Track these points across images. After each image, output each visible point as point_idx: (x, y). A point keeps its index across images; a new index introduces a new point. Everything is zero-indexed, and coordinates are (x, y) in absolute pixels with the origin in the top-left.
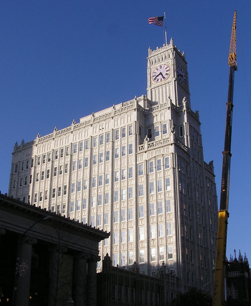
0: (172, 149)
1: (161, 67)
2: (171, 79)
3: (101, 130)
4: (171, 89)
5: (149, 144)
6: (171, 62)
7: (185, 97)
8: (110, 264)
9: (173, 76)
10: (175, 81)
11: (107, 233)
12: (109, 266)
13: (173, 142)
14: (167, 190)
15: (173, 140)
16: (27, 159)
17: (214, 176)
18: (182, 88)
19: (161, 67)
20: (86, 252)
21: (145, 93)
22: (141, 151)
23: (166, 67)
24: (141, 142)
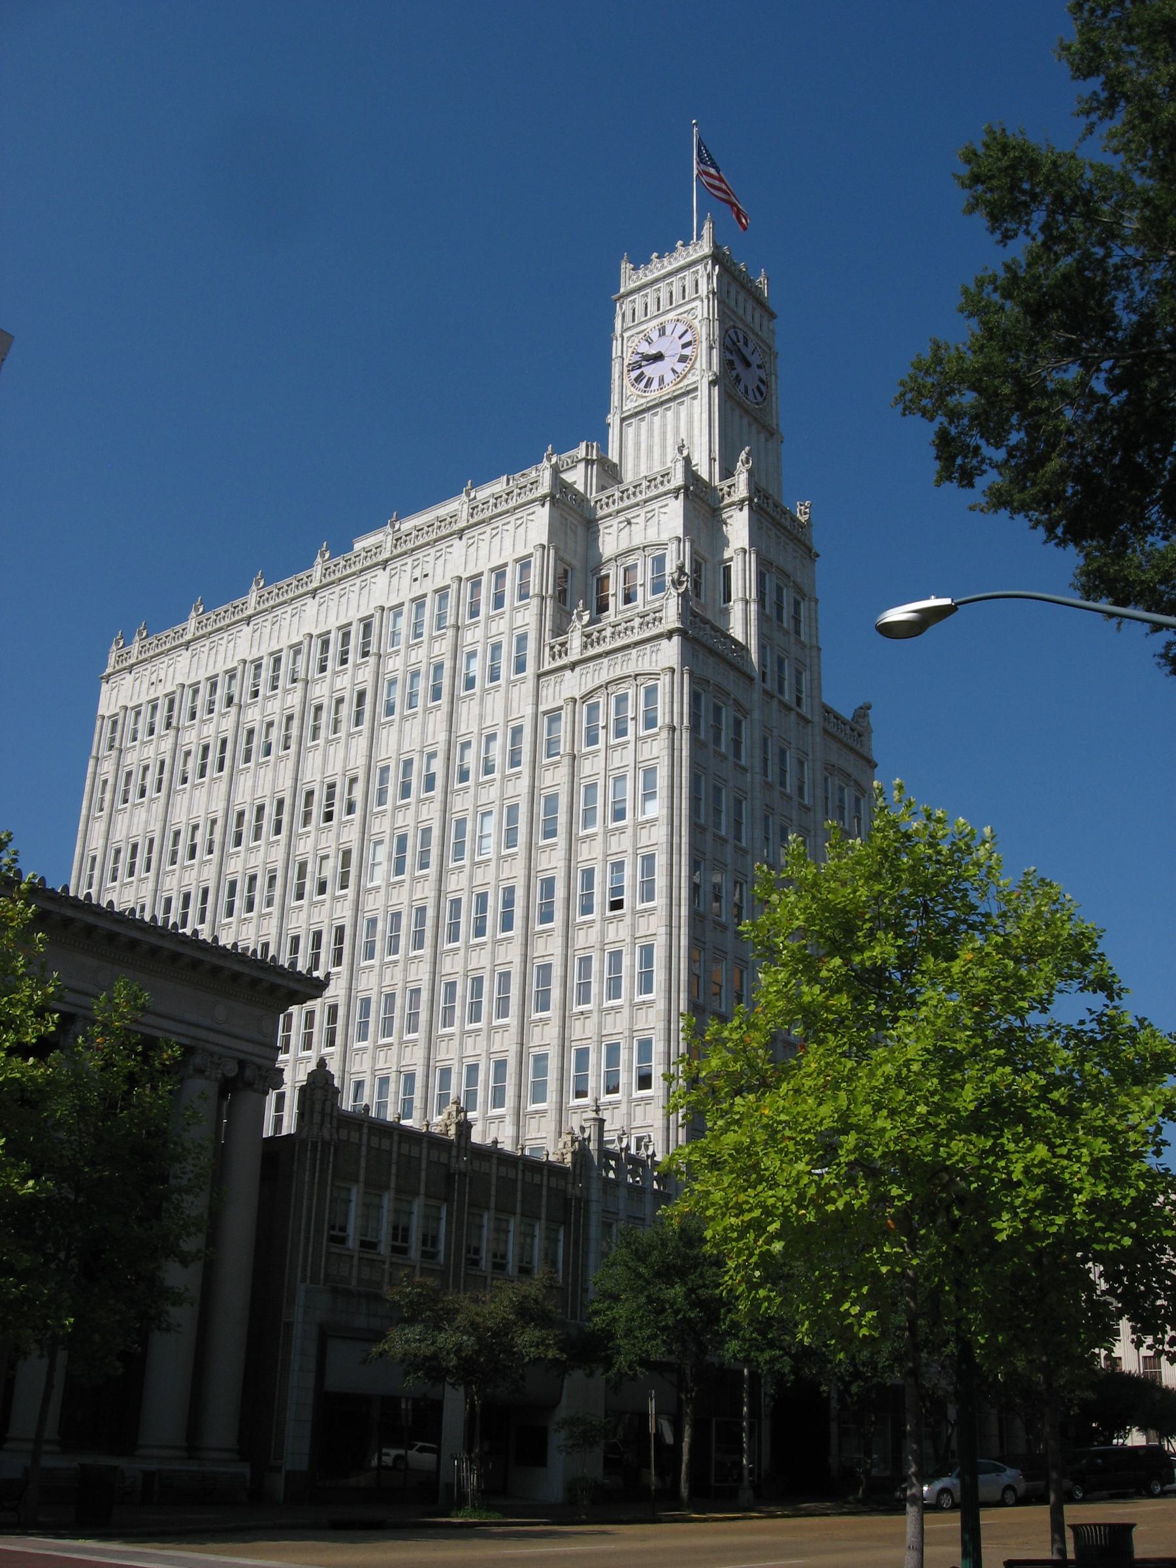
0: (670, 652)
1: (662, 331)
2: (699, 378)
3: (418, 582)
4: (696, 417)
5: (588, 636)
6: (699, 309)
7: (747, 448)
8: (328, 1104)
9: (704, 367)
10: (712, 383)
11: (312, 979)
12: (323, 1109)
13: (678, 625)
14: (645, 817)
15: (675, 617)
16: (153, 697)
17: (872, 765)
18: (747, 412)
19: (662, 331)
20: (216, 1049)
21: (600, 435)
22: (559, 663)
23: (681, 328)
24: (560, 629)
